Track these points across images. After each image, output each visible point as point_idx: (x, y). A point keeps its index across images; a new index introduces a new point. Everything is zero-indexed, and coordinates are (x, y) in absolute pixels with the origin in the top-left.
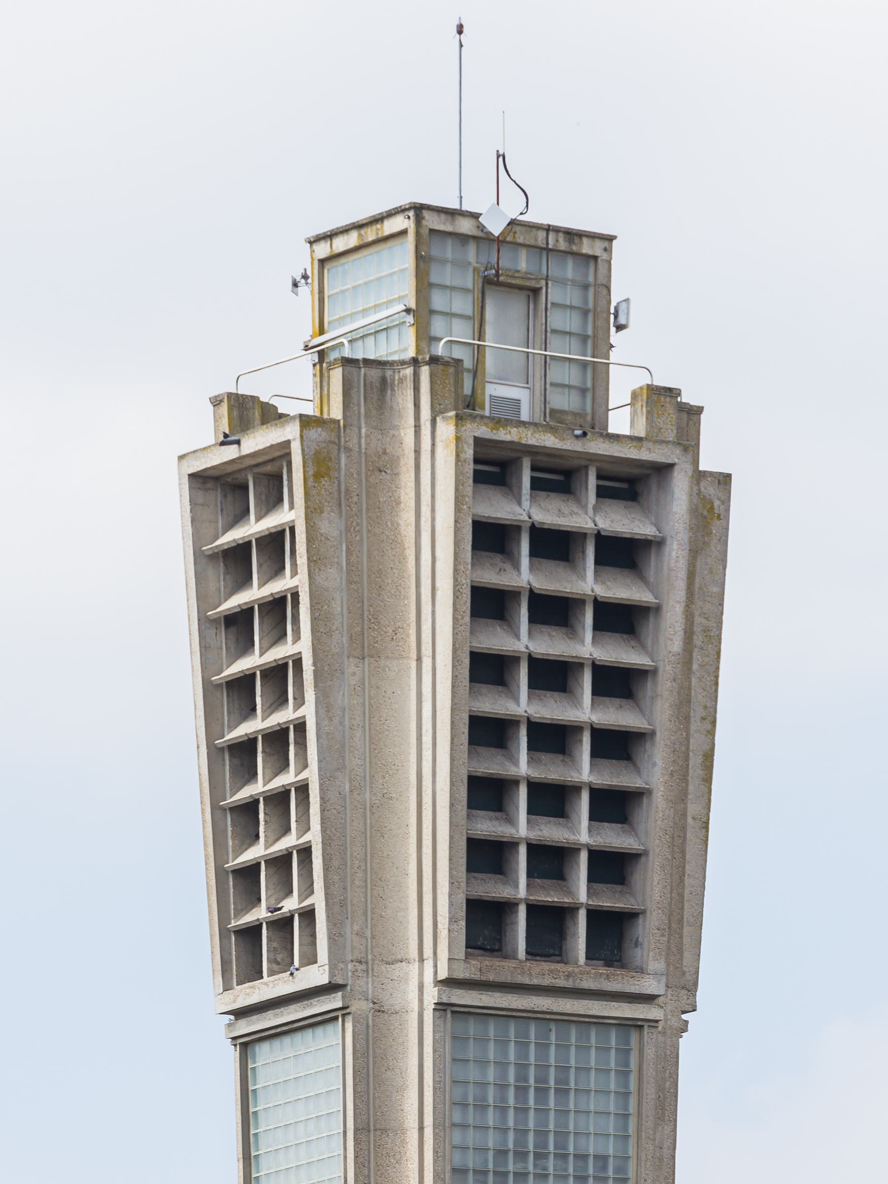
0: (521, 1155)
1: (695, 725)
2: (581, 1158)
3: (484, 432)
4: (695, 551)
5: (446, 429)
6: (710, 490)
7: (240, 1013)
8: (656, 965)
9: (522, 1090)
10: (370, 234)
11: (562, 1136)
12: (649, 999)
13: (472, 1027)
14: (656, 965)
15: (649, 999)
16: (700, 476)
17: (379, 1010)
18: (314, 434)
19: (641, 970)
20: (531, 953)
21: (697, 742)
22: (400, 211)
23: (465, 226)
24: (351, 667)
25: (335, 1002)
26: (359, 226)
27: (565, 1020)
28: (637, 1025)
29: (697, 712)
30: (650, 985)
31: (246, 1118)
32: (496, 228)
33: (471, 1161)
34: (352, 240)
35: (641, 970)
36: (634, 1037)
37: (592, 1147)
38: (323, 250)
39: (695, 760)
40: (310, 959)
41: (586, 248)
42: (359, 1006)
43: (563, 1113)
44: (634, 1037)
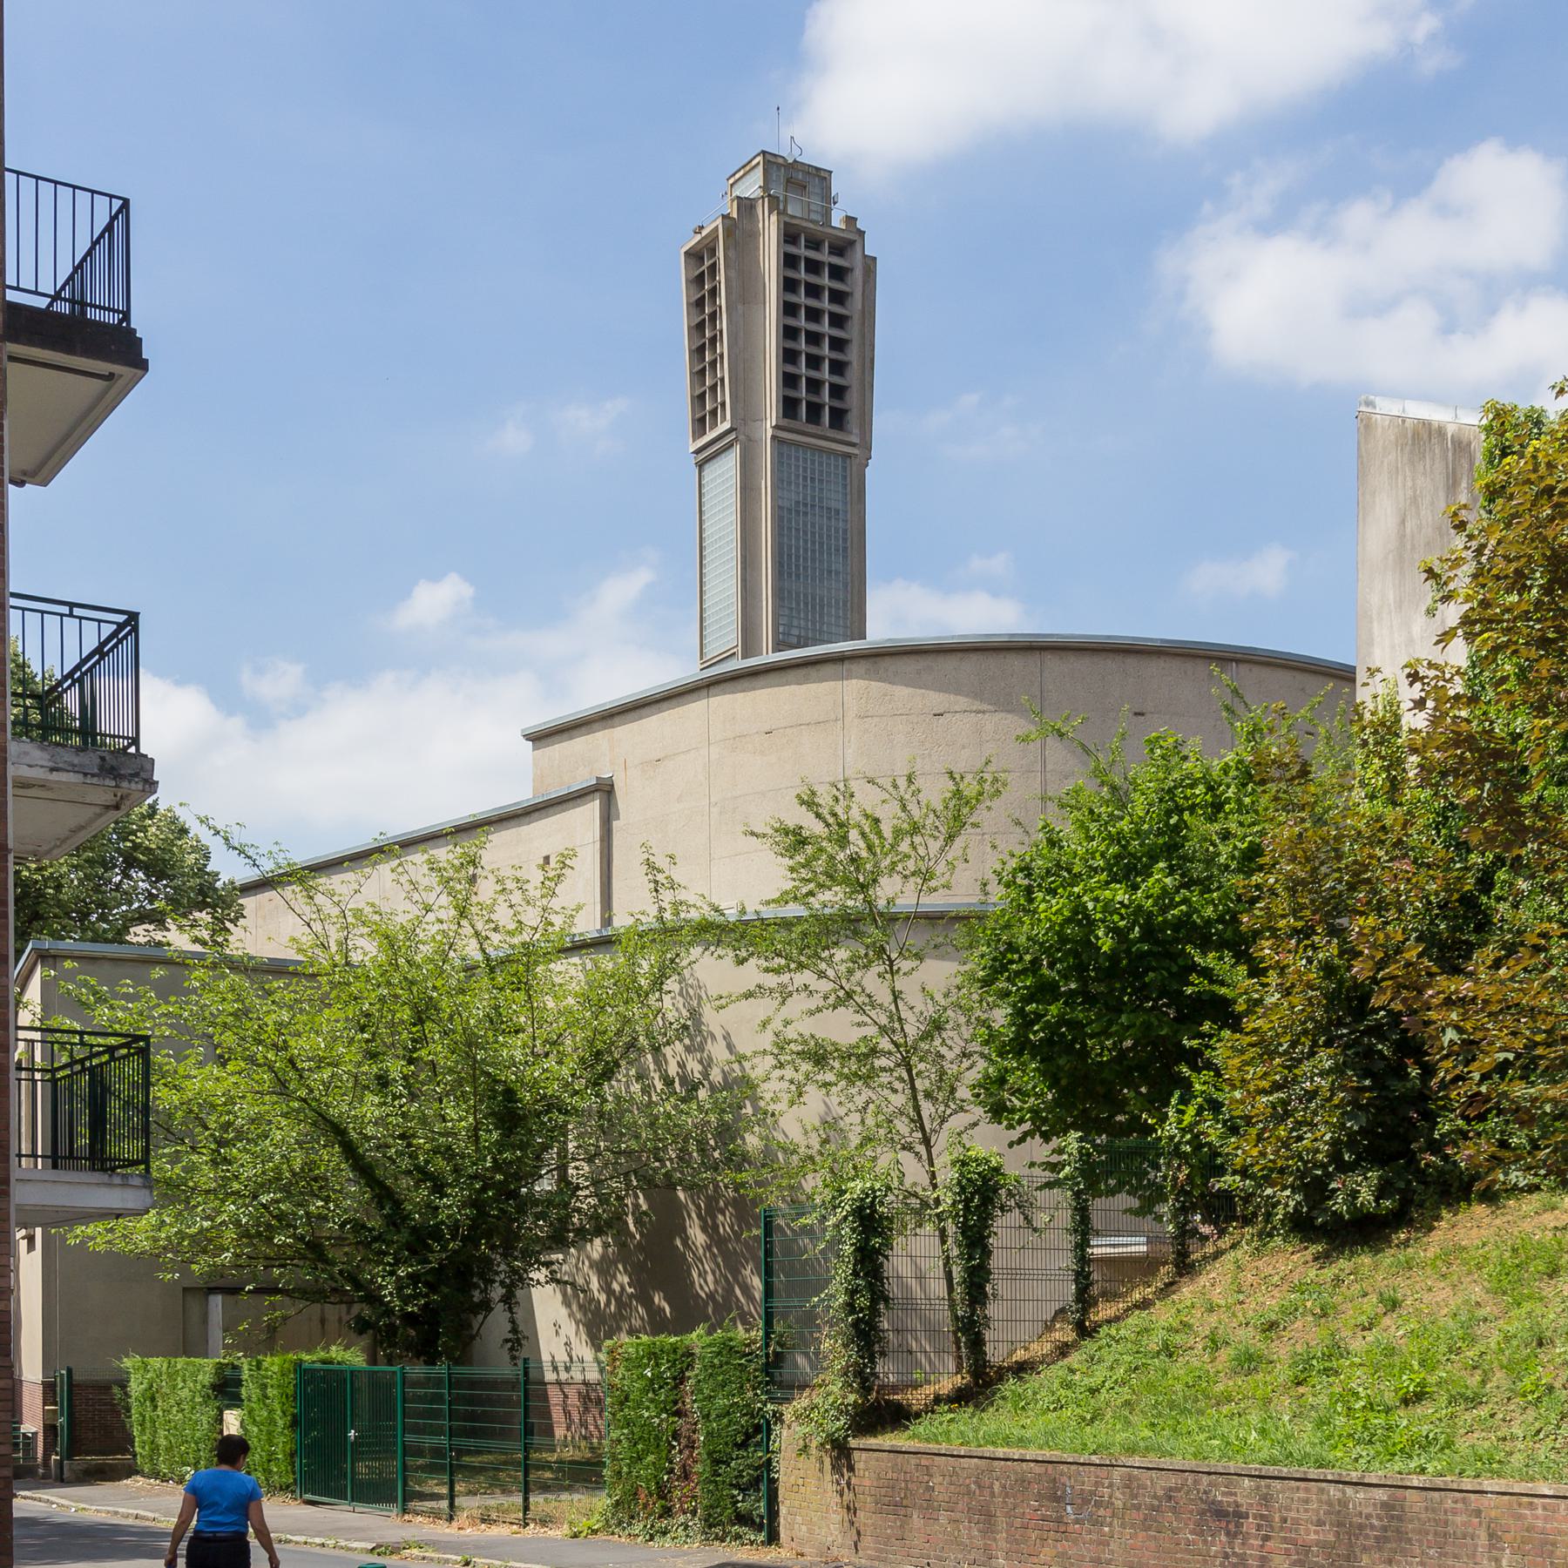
0: (805, 505)
1: (867, 347)
2: (829, 509)
3: (787, 219)
4: (864, 283)
5: (774, 218)
6: (869, 262)
7: (697, 452)
8: (856, 431)
9: (805, 478)
10: (748, 168)
11: (821, 500)
12: (853, 445)
13: (785, 448)
14: (856, 431)
15: (853, 445)
16: (865, 256)
17: (749, 439)
18: (726, 221)
19: (851, 433)
20: (807, 421)
21: (867, 379)
22: (758, 155)
23: (780, 161)
24: (740, 307)
25: (733, 436)
26: (744, 167)
27: (821, 450)
28: (848, 456)
29: (867, 342)
30: (855, 439)
31: (701, 557)
32: (790, 161)
33: (786, 504)
34: (742, 173)
35: (851, 433)
36: (848, 461)
37: (833, 505)
38: (731, 181)
39: (867, 360)
40: (724, 419)
41: (822, 174)
42: (742, 437)
43: (821, 490)
44: (848, 461)
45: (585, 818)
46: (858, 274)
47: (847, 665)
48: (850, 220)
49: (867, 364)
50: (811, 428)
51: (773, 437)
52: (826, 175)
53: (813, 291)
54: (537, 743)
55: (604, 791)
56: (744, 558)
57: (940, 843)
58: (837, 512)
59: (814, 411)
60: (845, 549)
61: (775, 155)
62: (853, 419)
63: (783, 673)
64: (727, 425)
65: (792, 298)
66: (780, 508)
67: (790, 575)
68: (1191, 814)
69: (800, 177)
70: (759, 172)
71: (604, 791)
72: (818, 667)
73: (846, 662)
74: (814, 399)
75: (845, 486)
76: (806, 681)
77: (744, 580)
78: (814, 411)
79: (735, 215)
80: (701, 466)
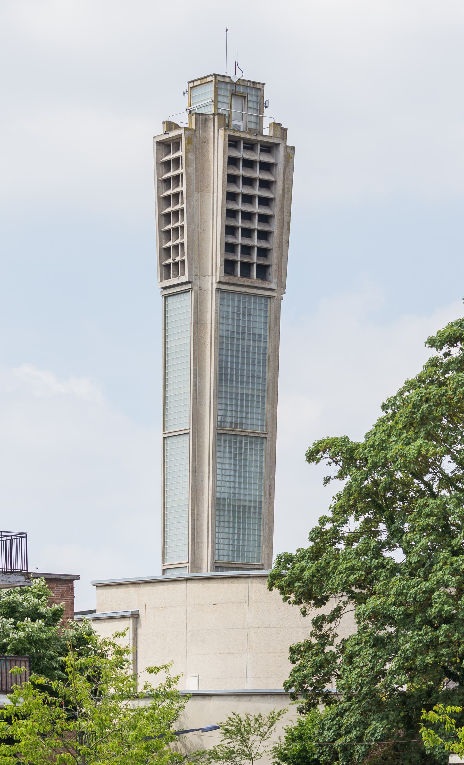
0: (238, 333)
1: (285, 214)
2: (254, 334)
3: (231, 133)
4: (285, 167)
5: (221, 132)
6: (289, 151)
7: (164, 288)
8: (275, 280)
10: (203, 81)
11: (249, 328)
13: (225, 295)
14: (275, 280)
16: (287, 147)
19: (271, 282)
23: (227, 80)
24: (196, 194)
25: (189, 286)
26: (200, 79)
27: (250, 295)
28: (269, 297)
29: (286, 211)
30: (273, 286)
33: (225, 334)
34: (198, 83)
35: (271, 282)
38: (191, 85)
39: (285, 224)
41: (258, 86)
43: (249, 321)
44: (269, 300)
45: (129, 623)
46: (280, 168)
47: (251, 579)
48: (276, 126)
49: (285, 227)
50: (244, 281)
51: (217, 289)
52: (260, 87)
53: (247, 233)
54: (99, 588)
55: (135, 616)
56: (195, 370)
57: (267, 728)
58: (260, 335)
59: (246, 267)
60: (265, 361)
61: (224, 77)
62: (273, 271)
63: (222, 580)
64: (184, 279)
65: (232, 257)
66: (221, 337)
67: (226, 381)
68: (449, 595)
69: (242, 90)
70: (211, 87)
71: (135, 616)
72: (238, 579)
73: (251, 579)
74: (247, 260)
75: (266, 311)
76: (233, 583)
77: (195, 386)
78: (246, 267)
79: (193, 127)
80: (166, 297)
